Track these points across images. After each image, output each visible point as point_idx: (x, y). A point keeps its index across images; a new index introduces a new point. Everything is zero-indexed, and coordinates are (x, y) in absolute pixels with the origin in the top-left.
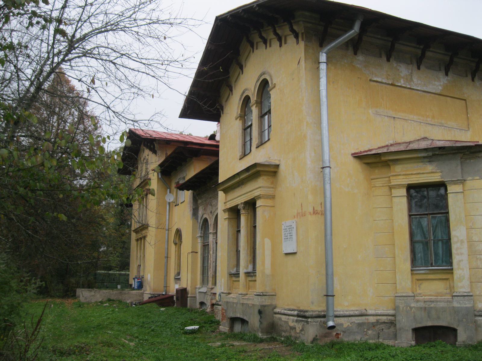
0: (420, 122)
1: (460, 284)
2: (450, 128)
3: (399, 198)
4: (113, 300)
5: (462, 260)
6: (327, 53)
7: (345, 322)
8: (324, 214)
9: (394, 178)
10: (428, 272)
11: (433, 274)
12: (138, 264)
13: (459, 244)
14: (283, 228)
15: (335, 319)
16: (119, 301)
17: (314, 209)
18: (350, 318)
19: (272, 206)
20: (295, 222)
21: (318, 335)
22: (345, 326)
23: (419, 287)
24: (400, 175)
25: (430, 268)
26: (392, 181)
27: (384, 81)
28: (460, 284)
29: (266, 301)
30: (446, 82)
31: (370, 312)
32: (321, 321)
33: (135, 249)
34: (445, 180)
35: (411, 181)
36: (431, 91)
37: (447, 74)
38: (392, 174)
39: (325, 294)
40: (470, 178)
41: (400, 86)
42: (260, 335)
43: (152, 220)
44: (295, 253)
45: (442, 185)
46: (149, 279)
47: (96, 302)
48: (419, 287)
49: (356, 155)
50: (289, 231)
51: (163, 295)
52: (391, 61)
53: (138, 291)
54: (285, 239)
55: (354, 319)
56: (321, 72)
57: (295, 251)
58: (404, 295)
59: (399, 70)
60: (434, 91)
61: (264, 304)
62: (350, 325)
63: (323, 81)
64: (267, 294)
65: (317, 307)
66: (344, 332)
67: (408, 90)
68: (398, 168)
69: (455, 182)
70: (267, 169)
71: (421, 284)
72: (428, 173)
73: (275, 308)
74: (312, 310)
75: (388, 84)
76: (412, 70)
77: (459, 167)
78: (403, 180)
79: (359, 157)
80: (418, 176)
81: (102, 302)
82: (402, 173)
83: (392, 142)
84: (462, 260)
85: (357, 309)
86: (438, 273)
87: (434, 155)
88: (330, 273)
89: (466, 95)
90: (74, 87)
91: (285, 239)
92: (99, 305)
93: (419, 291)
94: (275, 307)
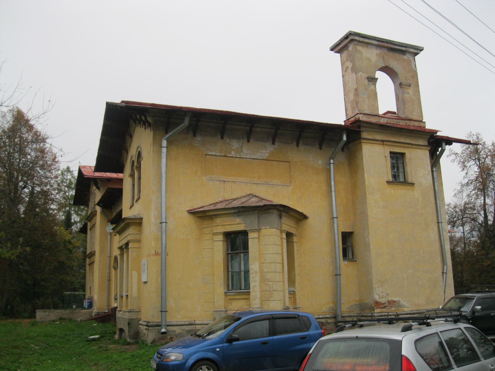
0: (247, 183)
1: (254, 302)
2: (273, 185)
3: (217, 242)
4: (64, 319)
5: (256, 286)
6: (167, 140)
7: (178, 330)
9: (216, 227)
10: (235, 294)
11: (239, 295)
12: (90, 286)
13: (254, 274)
15: (167, 327)
16: (69, 319)
17: (156, 252)
18: (181, 327)
19: (138, 248)
21: (156, 338)
22: (177, 332)
23: (231, 304)
24: (219, 225)
25: (239, 291)
26: (214, 230)
27: (217, 154)
28: (254, 302)
29: (134, 316)
30: (272, 149)
31: (197, 322)
32: (159, 329)
33: (89, 271)
34: (246, 229)
35: (226, 230)
36: (259, 158)
37: (273, 144)
38: (214, 225)
39: (160, 310)
40: (264, 228)
41: (232, 157)
42: (128, 340)
43: (97, 249)
45: (245, 233)
46: (96, 299)
47: (50, 321)
48: (231, 304)
49: (191, 211)
51: (106, 313)
52: (224, 138)
53: (87, 310)
55: (184, 327)
56: (163, 154)
57: (146, 281)
58: (219, 310)
59: (231, 144)
60: (261, 158)
61: (131, 318)
62: (182, 332)
63: (164, 160)
64: (134, 311)
65: (156, 320)
66: (177, 336)
67: (239, 159)
68: (219, 221)
69: (253, 231)
70: (134, 221)
71: (232, 302)
72: (236, 224)
73: (140, 321)
74: (152, 321)
75: (222, 156)
76: (242, 143)
77: (257, 220)
78: (221, 229)
79: (192, 213)
80: (230, 226)
81: (54, 321)
82: (220, 224)
83: (221, 200)
84: (256, 286)
85: (187, 320)
86: (241, 295)
87: (239, 212)
89: (290, 158)
90: (33, 125)
92: (52, 323)
93: (230, 307)
94: (140, 320)
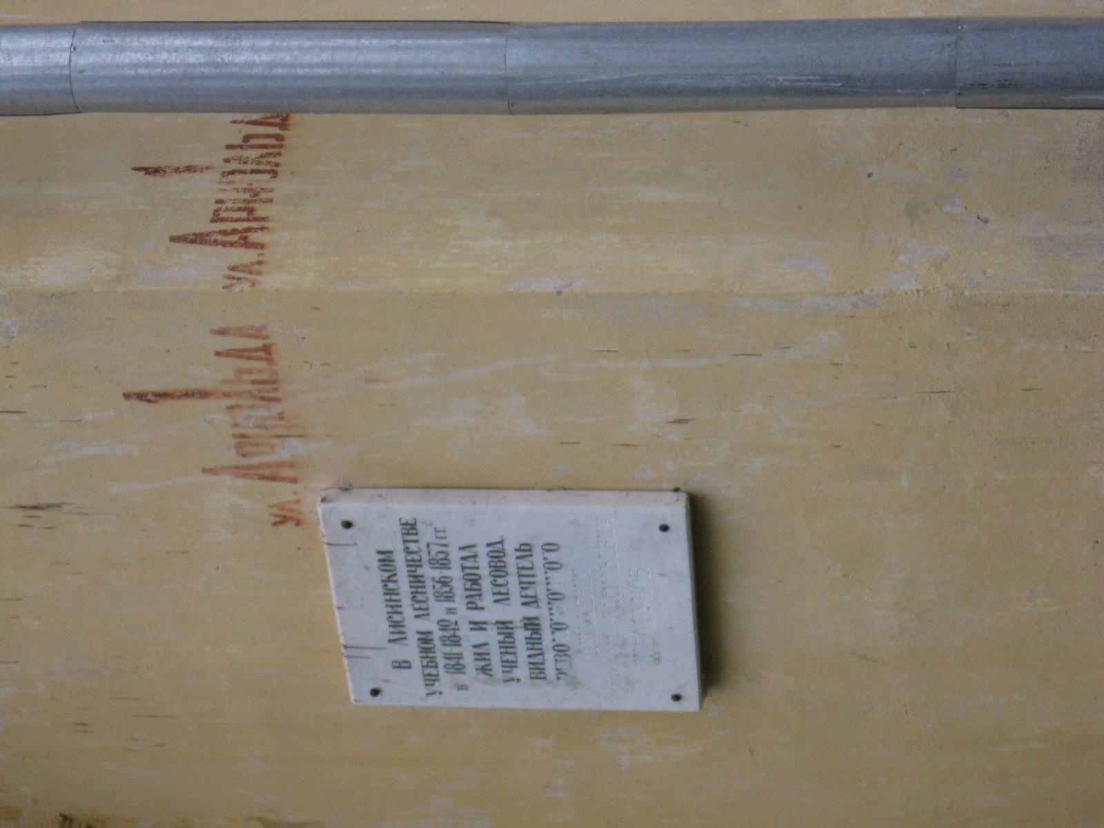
8: (271, 115)
14: (407, 691)
17: (199, 239)
20: (348, 507)
44: (701, 520)
50: (445, 591)
54: (537, 671)
57: (676, 513)
88: (928, 54)
91: (537, 671)
